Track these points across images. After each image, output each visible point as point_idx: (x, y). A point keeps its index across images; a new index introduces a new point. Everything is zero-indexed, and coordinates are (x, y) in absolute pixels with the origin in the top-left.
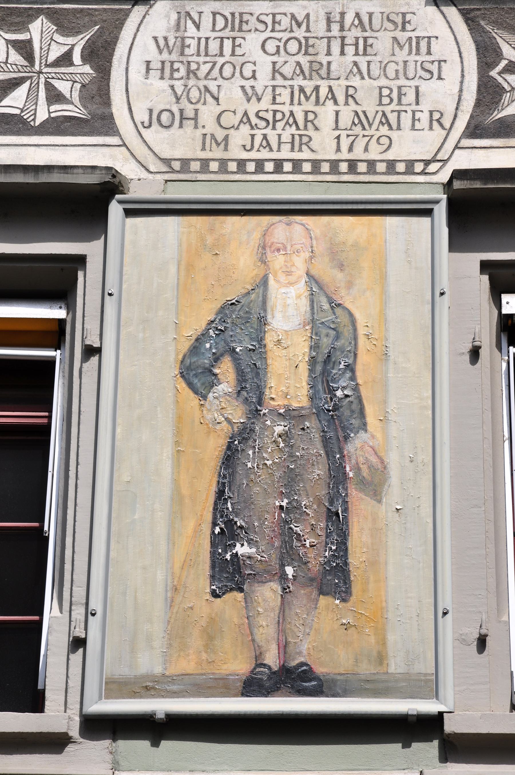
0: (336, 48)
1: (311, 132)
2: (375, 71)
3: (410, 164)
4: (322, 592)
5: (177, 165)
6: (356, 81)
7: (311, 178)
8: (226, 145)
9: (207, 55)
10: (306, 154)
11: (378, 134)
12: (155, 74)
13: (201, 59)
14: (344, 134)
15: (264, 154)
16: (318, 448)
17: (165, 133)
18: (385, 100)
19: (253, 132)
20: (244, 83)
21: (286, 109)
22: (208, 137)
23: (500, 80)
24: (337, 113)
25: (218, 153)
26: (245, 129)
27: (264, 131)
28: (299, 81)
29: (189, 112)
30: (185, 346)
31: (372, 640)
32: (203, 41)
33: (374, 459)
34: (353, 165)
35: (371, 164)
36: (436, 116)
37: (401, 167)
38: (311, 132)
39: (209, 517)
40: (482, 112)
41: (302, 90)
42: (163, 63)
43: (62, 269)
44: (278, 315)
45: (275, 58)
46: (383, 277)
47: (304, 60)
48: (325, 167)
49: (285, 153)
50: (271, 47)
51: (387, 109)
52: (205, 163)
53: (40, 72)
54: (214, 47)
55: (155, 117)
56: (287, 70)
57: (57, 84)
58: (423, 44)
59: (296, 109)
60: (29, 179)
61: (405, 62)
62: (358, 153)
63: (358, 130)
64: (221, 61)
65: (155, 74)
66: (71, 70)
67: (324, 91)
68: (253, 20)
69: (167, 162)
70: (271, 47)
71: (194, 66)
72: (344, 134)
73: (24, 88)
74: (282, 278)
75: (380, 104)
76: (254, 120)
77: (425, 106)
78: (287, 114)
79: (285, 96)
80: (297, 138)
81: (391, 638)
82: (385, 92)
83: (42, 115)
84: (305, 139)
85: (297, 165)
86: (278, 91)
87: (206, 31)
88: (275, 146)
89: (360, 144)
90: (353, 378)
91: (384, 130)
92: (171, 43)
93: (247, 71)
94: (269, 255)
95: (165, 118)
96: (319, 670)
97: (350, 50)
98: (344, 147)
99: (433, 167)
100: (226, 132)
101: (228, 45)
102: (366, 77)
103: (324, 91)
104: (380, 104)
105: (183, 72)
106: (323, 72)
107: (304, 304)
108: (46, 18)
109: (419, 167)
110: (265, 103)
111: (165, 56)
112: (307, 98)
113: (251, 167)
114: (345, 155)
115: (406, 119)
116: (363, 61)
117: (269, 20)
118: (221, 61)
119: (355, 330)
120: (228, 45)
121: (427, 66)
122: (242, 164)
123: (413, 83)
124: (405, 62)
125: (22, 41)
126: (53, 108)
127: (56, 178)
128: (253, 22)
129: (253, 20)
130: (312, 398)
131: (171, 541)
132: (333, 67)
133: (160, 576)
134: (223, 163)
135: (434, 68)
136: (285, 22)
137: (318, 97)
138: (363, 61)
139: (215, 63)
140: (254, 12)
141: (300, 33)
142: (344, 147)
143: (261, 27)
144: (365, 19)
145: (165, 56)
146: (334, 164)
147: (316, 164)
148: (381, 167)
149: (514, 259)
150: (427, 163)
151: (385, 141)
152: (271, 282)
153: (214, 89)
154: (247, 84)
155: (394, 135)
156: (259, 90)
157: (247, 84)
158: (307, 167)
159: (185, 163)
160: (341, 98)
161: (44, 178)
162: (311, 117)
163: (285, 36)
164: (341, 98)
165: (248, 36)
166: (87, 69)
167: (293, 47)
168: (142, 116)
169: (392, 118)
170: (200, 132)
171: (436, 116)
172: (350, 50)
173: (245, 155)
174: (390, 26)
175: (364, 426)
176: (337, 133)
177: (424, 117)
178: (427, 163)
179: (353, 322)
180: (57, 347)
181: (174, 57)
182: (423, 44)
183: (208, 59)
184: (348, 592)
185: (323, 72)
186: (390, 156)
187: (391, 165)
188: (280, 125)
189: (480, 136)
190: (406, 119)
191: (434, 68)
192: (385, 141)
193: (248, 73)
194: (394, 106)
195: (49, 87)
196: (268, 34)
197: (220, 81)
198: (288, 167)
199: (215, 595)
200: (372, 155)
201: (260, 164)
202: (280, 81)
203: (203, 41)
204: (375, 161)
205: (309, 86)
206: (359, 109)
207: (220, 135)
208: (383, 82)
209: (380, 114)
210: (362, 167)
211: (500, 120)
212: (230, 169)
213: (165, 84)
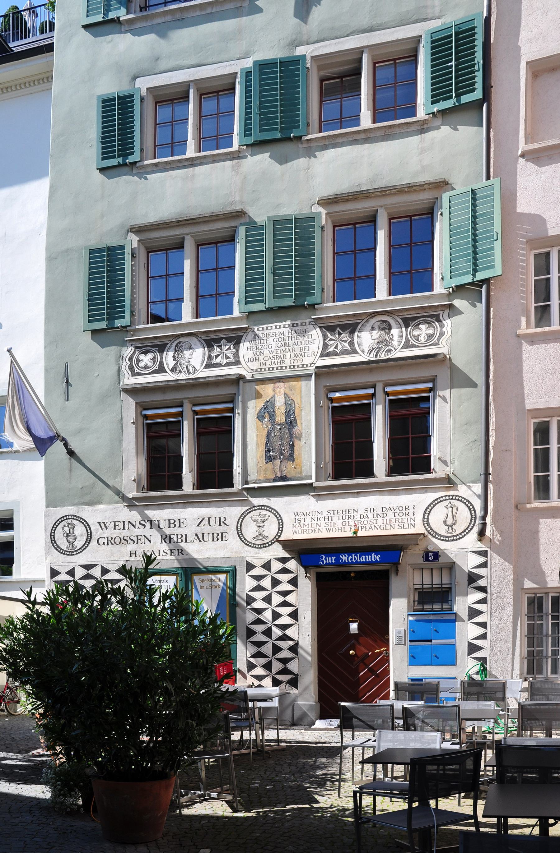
0: (290, 339)
1: (285, 360)
2: (299, 343)
3: (307, 365)
4: (288, 461)
5: (255, 370)
7: (285, 370)
10: (284, 365)
12: (249, 350)
13: (259, 345)
14: (292, 359)
15: (274, 366)
16: (287, 431)
17: (252, 363)
18: (302, 350)
21: (279, 355)
23: (328, 343)
25: (264, 367)
26: (270, 360)
28: (282, 348)
30: (257, 411)
31: (299, 470)
33: (299, 432)
34: (294, 366)
35: (298, 366)
36: (313, 353)
37: (305, 366)
38: (285, 359)
39: (264, 447)
41: (282, 350)
44: (278, 403)
46: (301, 392)
47: (283, 343)
48: (288, 367)
49: (279, 365)
50: (275, 340)
51: (302, 352)
52: (261, 369)
56: (279, 346)
57: (227, 354)
58: (310, 336)
59: (281, 354)
60: (221, 378)
62: (295, 364)
64: (264, 345)
65: (249, 350)
66: (230, 351)
67: (287, 350)
69: (252, 370)
70: (275, 340)
71: (258, 347)
72: (292, 359)
73: (221, 356)
74: (278, 394)
76: (272, 358)
77: (311, 351)
81: (303, 469)
82: (301, 348)
83: (225, 362)
85: (281, 367)
88: (276, 364)
89: (296, 361)
90: (294, 415)
91: (301, 357)
94: (276, 389)
95: (252, 360)
96: (288, 476)
97: (293, 339)
98: (292, 362)
99: (312, 365)
101: (265, 341)
102: (202, 540)
103: (287, 350)
105: (255, 349)
106: (287, 345)
107: (284, 400)
109: (309, 365)
110: (274, 354)
111: (251, 345)
113: (271, 369)
114: (292, 364)
116: (296, 341)
117: (275, 334)
118: (264, 345)
119: (295, 404)
121: (311, 341)
122: (269, 369)
123: (308, 346)
126: (227, 360)
127: (227, 377)
129: (271, 334)
130: (286, 420)
131: (257, 452)
132: (290, 343)
133: (255, 460)
134: (265, 369)
136: (278, 334)
138: (296, 341)
140: (407, 543)
141: (282, 336)
142: (292, 362)
143: (273, 336)
144: (297, 331)
146: (290, 366)
147: (286, 367)
149: (6, 192)
150: (311, 364)
151: (301, 360)
152: (276, 395)
153: (262, 352)
154: (270, 350)
155: (303, 358)
156: (273, 351)
157: (270, 350)
158: (284, 368)
159: (256, 370)
160: (291, 351)
161: (225, 378)
162: (285, 356)
163: (279, 337)
164: (291, 351)
165: (270, 338)
166: (234, 350)
167: (280, 340)
168: (247, 360)
169: (303, 354)
171: (313, 353)
172: (293, 339)
173: (270, 367)
175: (297, 425)
177: (310, 354)
178: (311, 364)
179: (294, 402)
181: (253, 345)
182: (310, 336)
184: (294, 460)
185: (287, 345)
186: (302, 363)
187: (303, 365)
188: (277, 359)
189: (323, 357)
191: (313, 341)
192: (301, 360)
193: (270, 347)
194: (303, 352)
196: (275, 337)
197: (264, 350)
198: (279, 368)
199: (266, 463)
200: (298, 364)
201: (273, 368)
202: (277, 348)
205: (284, 349)
206: (295, 353)
208: (301, 346)
210: (296, 367)
213: (252, 351)
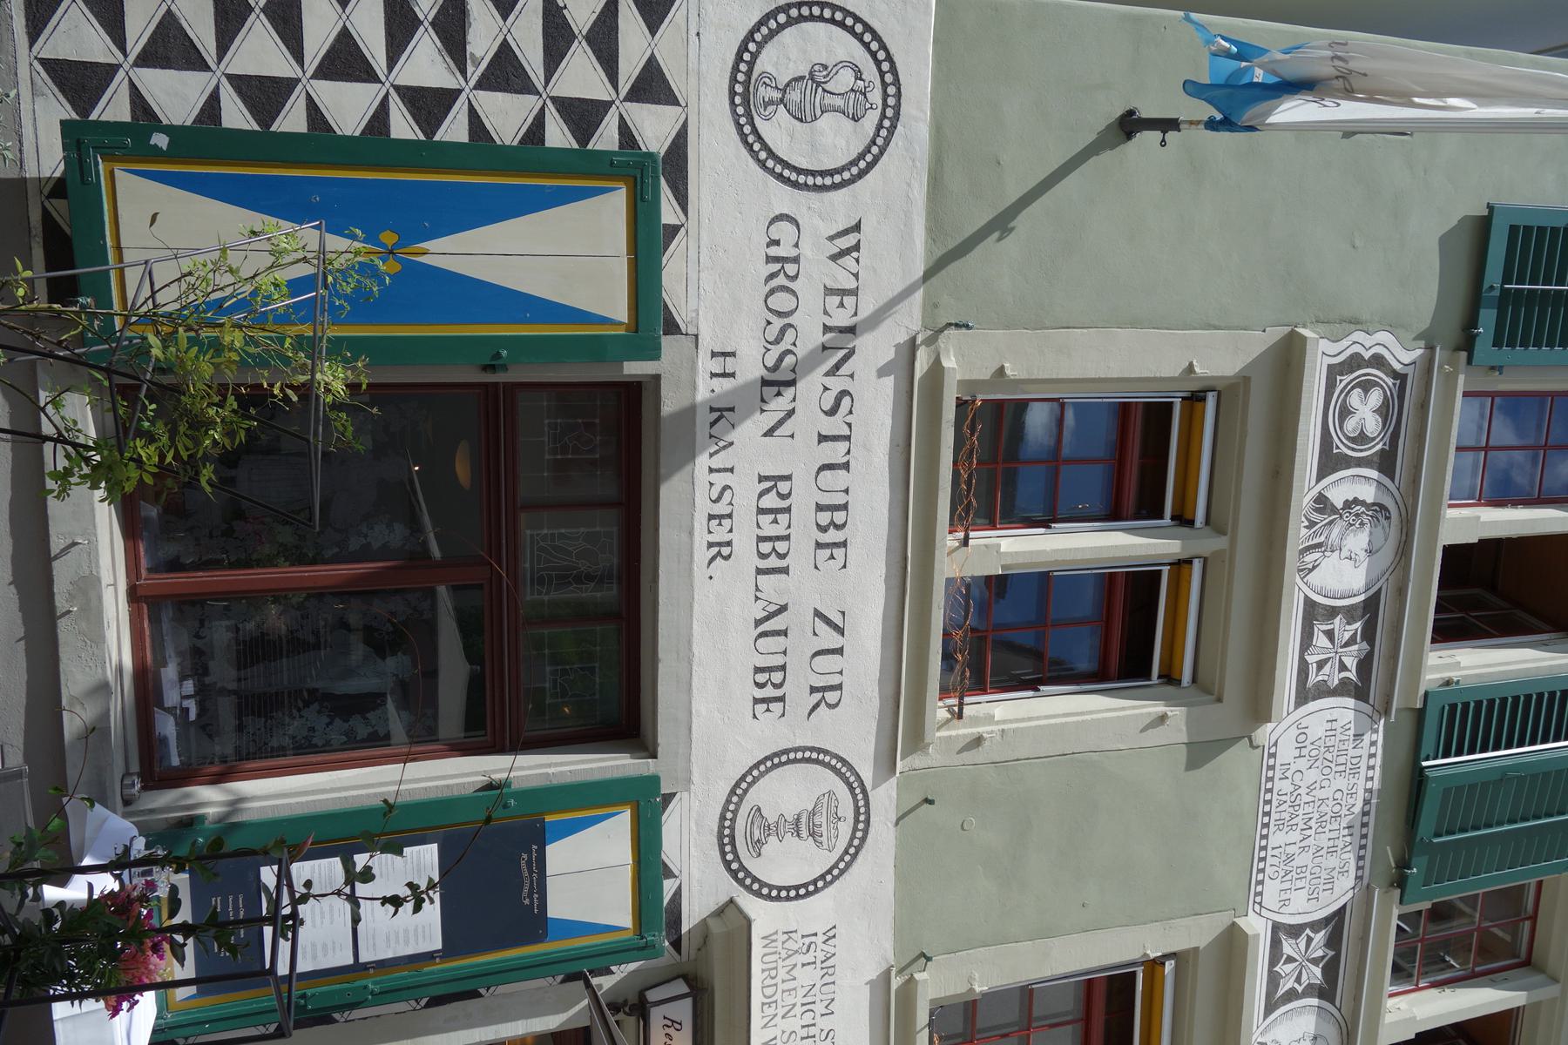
0: (1333, 835)
3: (1261, 894)
6: (1313, 850)
8: (1283, 779)
9: (1338, 756)
11: (1280, 870)
12: (1329, 726)
15: (1275, 803)
19: (1289, 794)
20: (1318, 782)
21: (1301, 812)
22: (1288, 767)
24: (1295, 843)
26: (1292, 788)
27: (1288, 801)
28: (1316, 816)
29: (1304, 751)
32: (1345, 752)
40: (1286, 929)
42: (1335, 730)
43: (1223, 561)
45: (1331, 799)
49: (1274, 816)
51: (1294, 873)
53: (1336, 653)
54: (1342, 760)
55: (1303, 731)
57: (1329, 664)
61: (1320, 877)
63: (1284, 858)
64: (1333, 765)
68: (1355, 781)
69: (1276, 744)
70: (1338, 796)
71: (1331, 749)
75: (1297, 868)
76: (1295, 794)
78: (1297, 813)
79: (1308, 809)
80: (1282, 822)
84: (1281, 827)
86: (1312, 804)
87: (1352, 753)
89: (1275, 861)
92: (1347, 733)
93: (1325, 783)
95: (1302, 738)
97: (1331, 843)
100: (1290, 778)
101: (1342, 768)
104: (1297, 868)
108: (1368, 653)
110: (1306, 798)
112: (1305, 824)
115: (1287, 885)
120: (1342, 768)
124: (1320, 877)
125: (1286, 959)
128: (1353, 781)
129: (1355, 781)
135: (1315, 895)
137: (1305, 829)
139: (1331, 762)
145: (1340, 730)
148: (1266, 820)
150: (1260, 904)
157: (1317, 785)
163: (1343, 803)
166: (1336, 682)
168: (1304, 723)
170: (1292, 761)
174: (1342, 865)
176: (1283, 845)
178: (1260, 904)
180: (1173, 518)
182: (1330, 886)
183: (1335, 758)
190: (1287, 885)
191: (1315, 895)
195: (1326, 661)
196: (1345, 792)
203: (1345, 752)
204: (1264, 873)
207: (1288, 774)
209: (1291, 869)
211: (1281, 941)
212: (1270, 798)
